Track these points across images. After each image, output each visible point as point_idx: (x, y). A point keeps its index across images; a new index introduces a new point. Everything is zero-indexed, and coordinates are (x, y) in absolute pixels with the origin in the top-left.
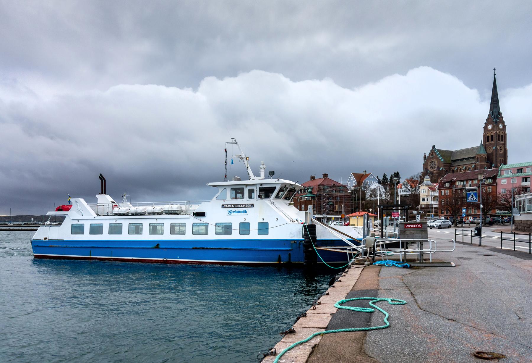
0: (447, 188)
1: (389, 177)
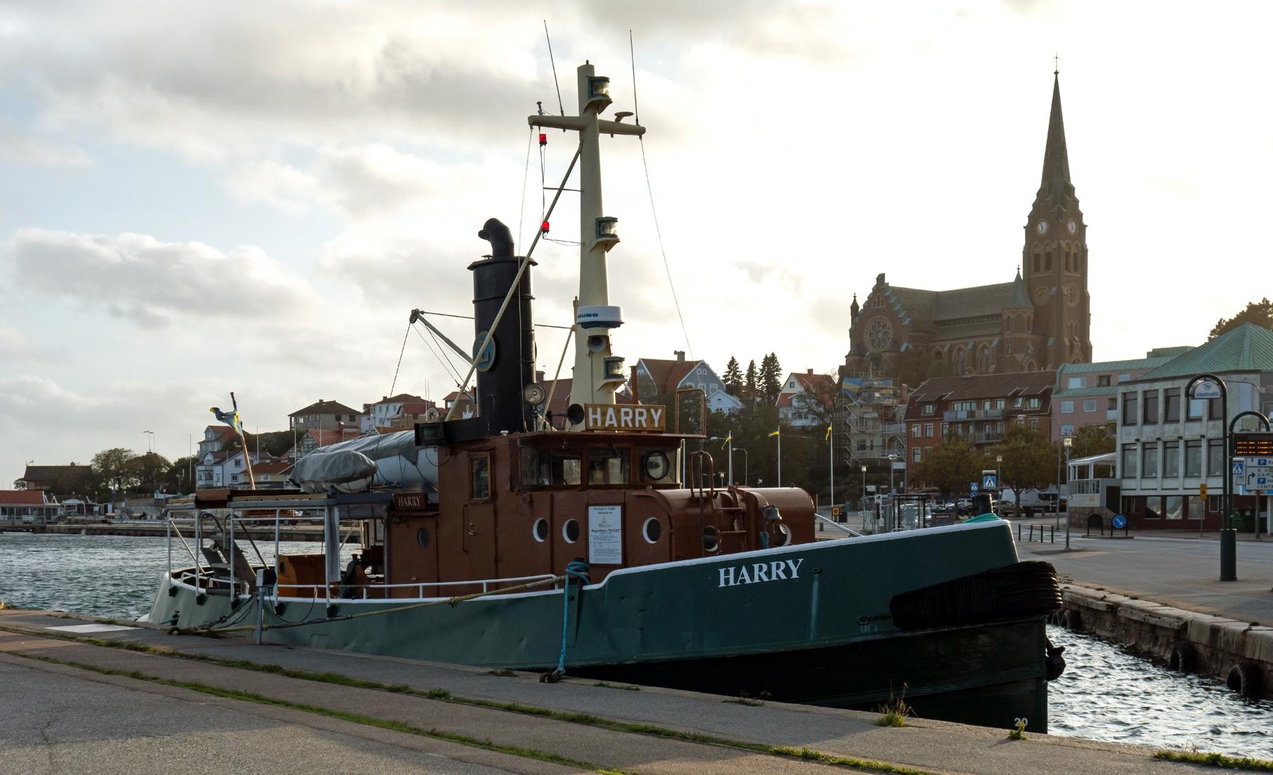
0: (928, 419)
1: (743, 369)
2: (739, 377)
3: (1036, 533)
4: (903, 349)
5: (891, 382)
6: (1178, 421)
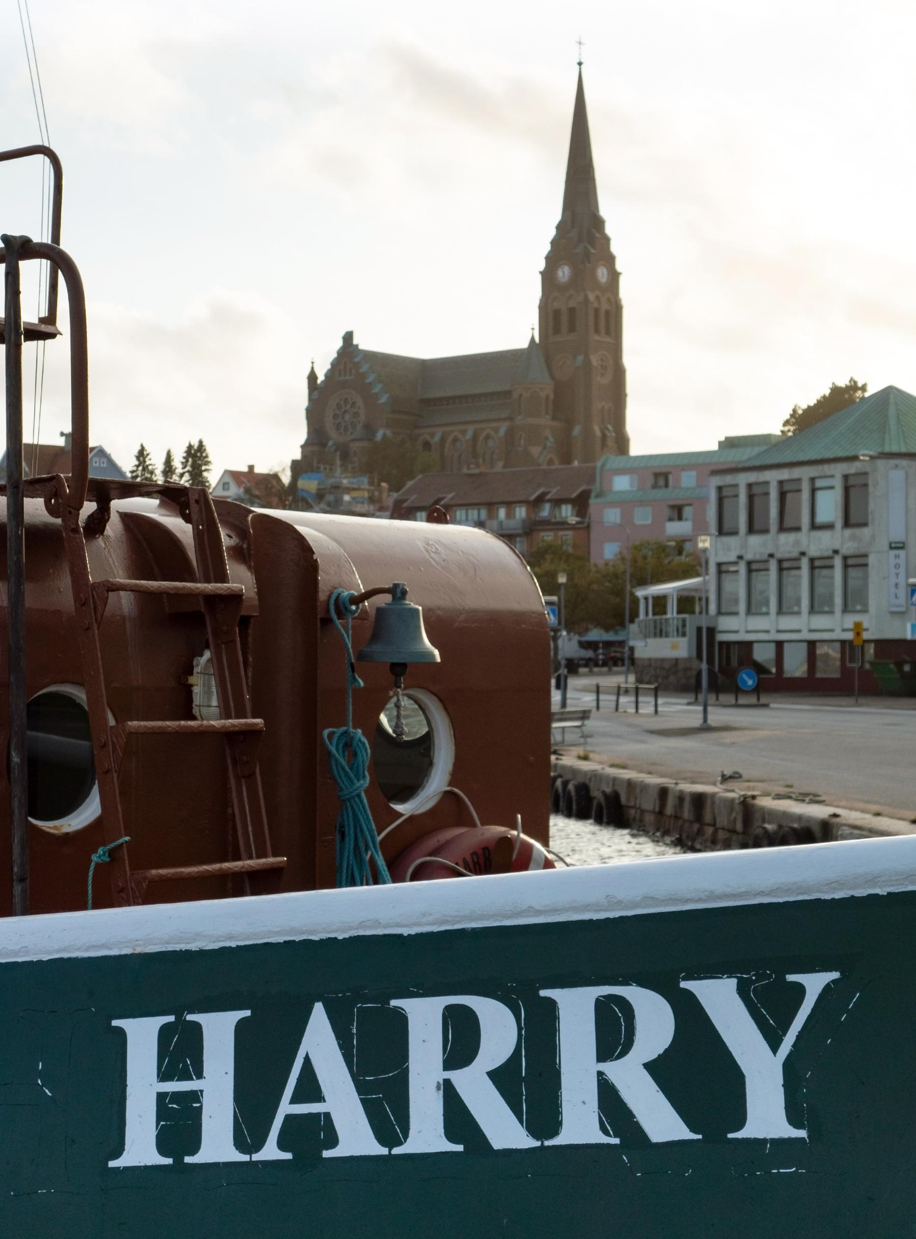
1: (157, 462)
2: (152, 473)
3: (608, 700)
4: (379, 436)
5: (365, 480)
6: (798, 529)
